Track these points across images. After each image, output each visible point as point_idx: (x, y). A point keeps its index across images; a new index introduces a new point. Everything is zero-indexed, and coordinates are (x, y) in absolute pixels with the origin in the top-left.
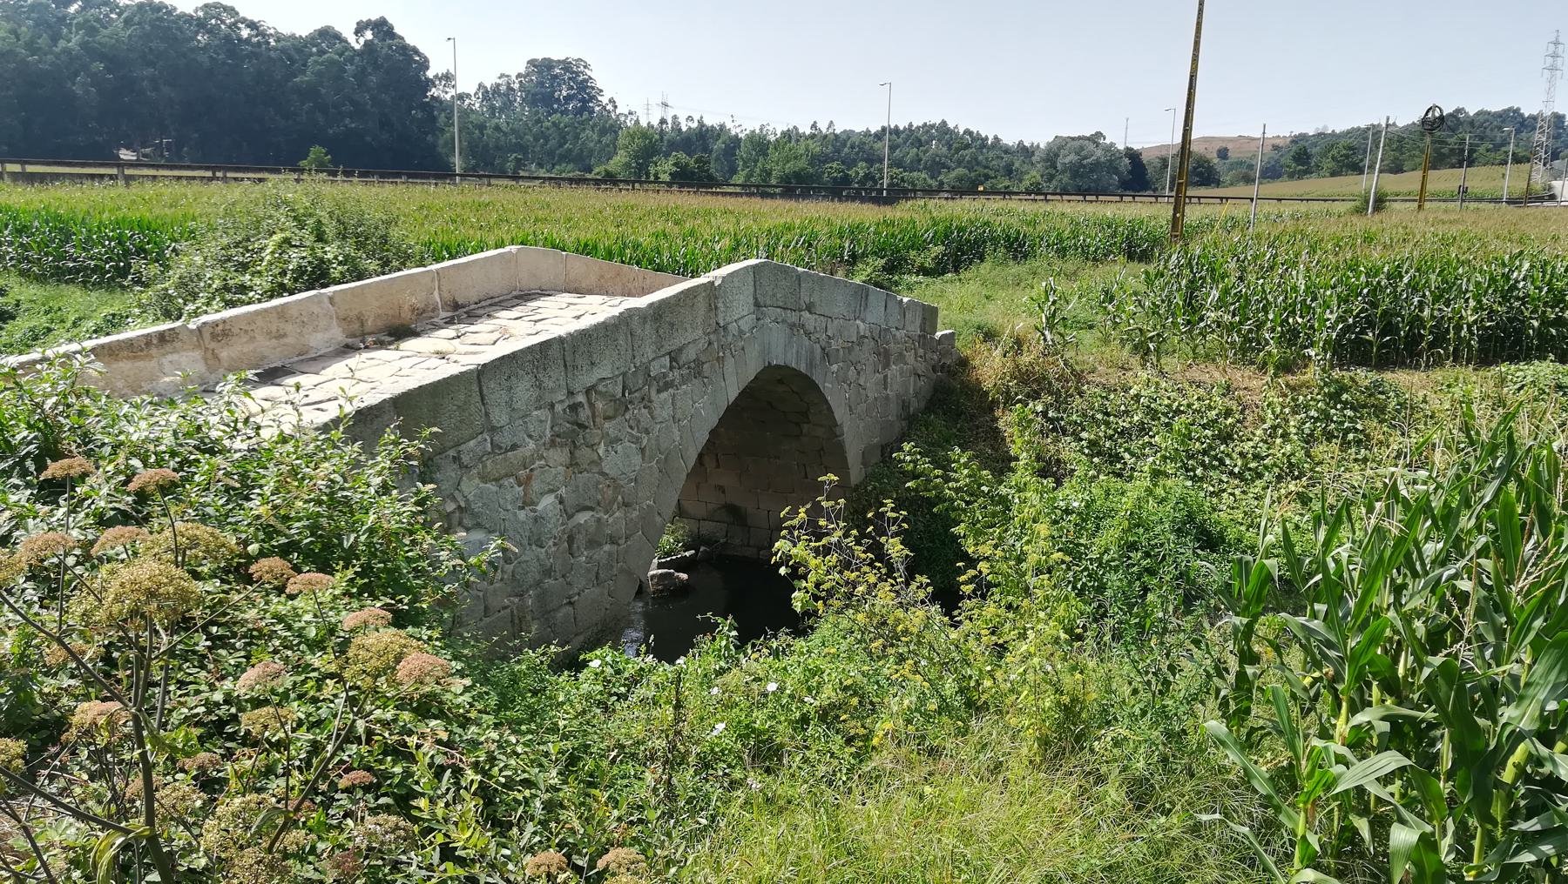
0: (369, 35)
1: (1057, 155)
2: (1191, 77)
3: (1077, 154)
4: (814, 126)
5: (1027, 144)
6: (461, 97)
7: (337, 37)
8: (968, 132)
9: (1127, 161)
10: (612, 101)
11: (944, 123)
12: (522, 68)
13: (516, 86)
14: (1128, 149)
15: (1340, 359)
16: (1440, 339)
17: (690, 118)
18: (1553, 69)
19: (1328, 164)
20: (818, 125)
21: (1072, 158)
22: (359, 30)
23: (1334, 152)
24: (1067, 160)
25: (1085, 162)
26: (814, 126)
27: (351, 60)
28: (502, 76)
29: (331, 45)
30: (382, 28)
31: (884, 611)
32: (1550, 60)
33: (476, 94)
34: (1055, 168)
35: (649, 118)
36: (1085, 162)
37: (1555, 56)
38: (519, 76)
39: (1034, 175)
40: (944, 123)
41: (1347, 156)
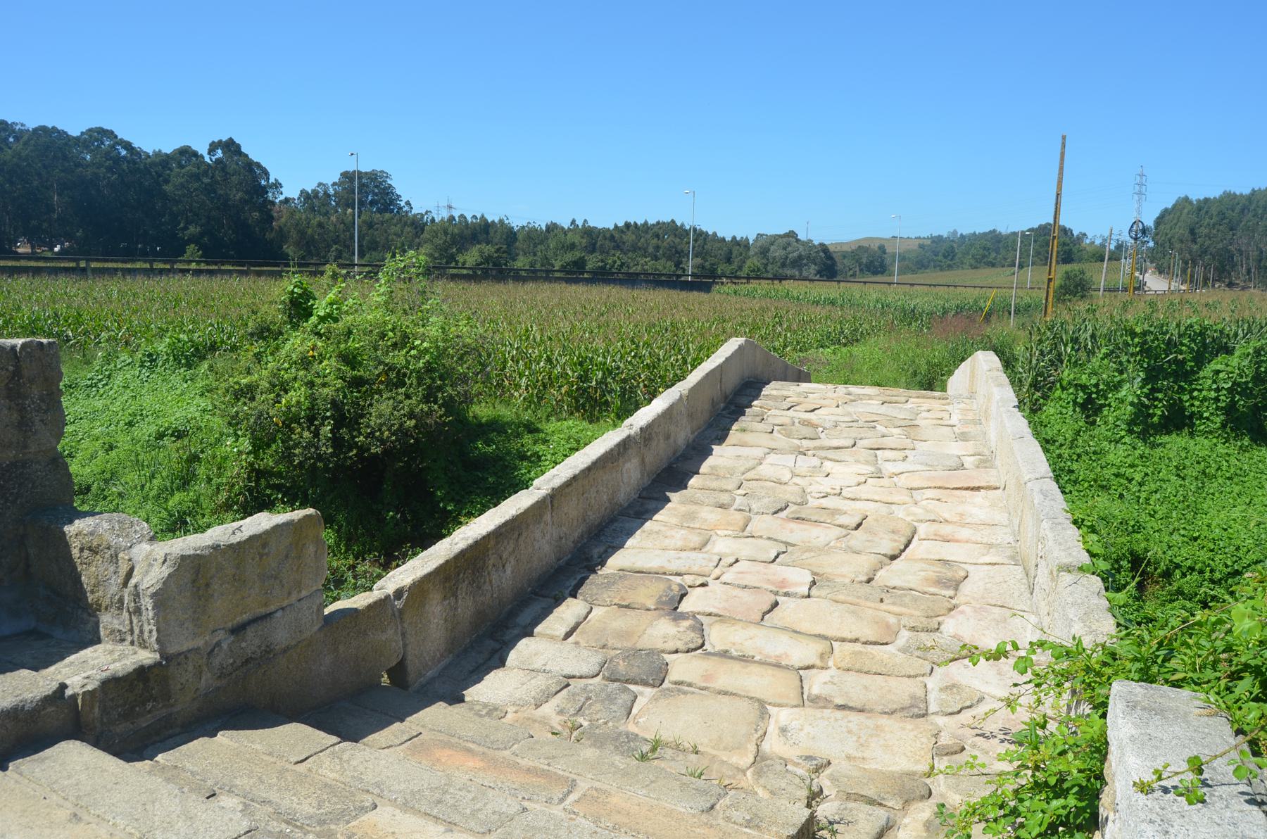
0: (219, 154)
2: (1057, 204)
4: (573, 222)
6: (287, 200)
7: (195, 154)
10: (408, 203)
12: (336, 178)
13: (331, 191)
14: (822, 245)
16: (399, 673)
17: (474, 217)
18: (1140, 193)
19: (969, 260)
20: (577, 223)
22: (212, 150)
26: (573, 222)
27: (205, 173)
28: (320, 184)
29: (189, 160)
30: (231, 147)
31: (1235, 535)
32: (1137, 187)
33: (299, 198)
35: (441, 215)
37: (1141, 185)
38: (334, 184)
39: (754, 262)
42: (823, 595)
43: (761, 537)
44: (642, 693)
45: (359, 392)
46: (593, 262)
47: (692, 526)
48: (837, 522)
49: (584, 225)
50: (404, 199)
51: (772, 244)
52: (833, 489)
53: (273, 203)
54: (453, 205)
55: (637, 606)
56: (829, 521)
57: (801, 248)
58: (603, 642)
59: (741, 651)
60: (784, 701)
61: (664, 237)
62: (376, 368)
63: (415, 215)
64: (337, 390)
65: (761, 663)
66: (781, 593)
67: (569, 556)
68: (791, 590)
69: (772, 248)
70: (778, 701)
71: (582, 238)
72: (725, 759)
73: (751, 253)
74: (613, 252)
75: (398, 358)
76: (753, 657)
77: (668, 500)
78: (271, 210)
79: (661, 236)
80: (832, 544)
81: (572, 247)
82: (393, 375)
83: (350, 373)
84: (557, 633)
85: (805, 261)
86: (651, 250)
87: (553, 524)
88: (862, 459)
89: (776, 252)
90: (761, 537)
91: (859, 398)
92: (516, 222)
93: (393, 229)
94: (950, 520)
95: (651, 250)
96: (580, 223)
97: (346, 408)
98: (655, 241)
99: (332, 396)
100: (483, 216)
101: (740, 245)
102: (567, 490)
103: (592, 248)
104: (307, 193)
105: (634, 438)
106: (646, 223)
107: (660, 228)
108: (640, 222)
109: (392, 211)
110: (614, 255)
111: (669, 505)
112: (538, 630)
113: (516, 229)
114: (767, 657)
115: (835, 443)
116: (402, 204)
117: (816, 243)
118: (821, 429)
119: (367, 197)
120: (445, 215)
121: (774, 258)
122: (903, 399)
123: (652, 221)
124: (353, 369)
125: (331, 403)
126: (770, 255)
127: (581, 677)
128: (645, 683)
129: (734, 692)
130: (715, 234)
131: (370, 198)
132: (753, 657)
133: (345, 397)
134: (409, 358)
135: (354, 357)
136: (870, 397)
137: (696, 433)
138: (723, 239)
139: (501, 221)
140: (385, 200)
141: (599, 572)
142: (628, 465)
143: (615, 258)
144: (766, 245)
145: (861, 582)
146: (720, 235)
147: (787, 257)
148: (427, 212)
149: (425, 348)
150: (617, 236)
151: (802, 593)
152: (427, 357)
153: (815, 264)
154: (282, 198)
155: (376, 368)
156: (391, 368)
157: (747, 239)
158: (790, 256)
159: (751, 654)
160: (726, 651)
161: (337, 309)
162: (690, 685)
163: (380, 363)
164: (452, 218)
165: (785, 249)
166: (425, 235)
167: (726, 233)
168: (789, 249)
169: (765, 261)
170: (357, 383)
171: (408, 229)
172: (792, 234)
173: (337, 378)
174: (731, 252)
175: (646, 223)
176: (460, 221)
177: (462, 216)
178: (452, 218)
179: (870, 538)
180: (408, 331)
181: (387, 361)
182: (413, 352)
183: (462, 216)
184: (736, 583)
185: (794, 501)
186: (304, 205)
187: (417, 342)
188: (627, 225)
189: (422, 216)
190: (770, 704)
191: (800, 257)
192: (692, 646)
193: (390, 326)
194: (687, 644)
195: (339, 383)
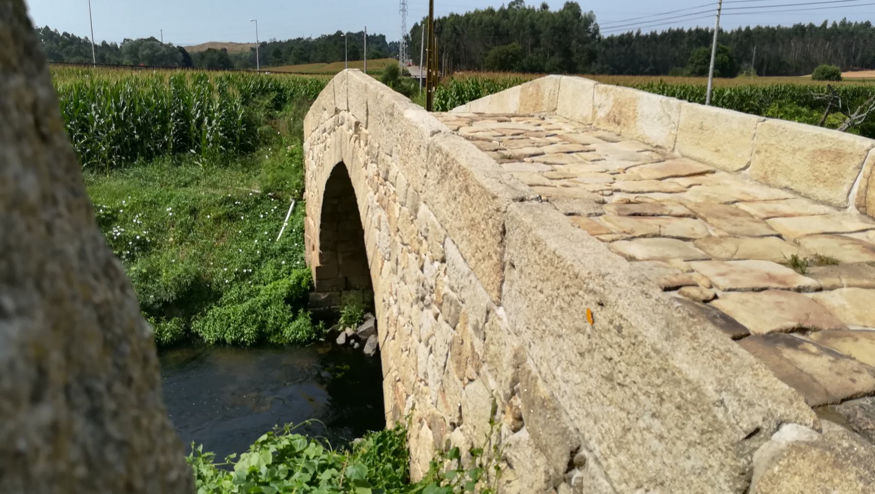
1: (137, 50)
3: (150, 49)
5: (109, 43)
8: (65, 34)
9: (181, 54)
11: (47, 28)
15: (125, 239)
19: (292, 57)
21: (147, 52)
23: (294, 51)
24: (145, 53)
25: (156, 54)
34: (137, 57)
36: (156, 54)
40: (47, 28)
41: (301, 54)
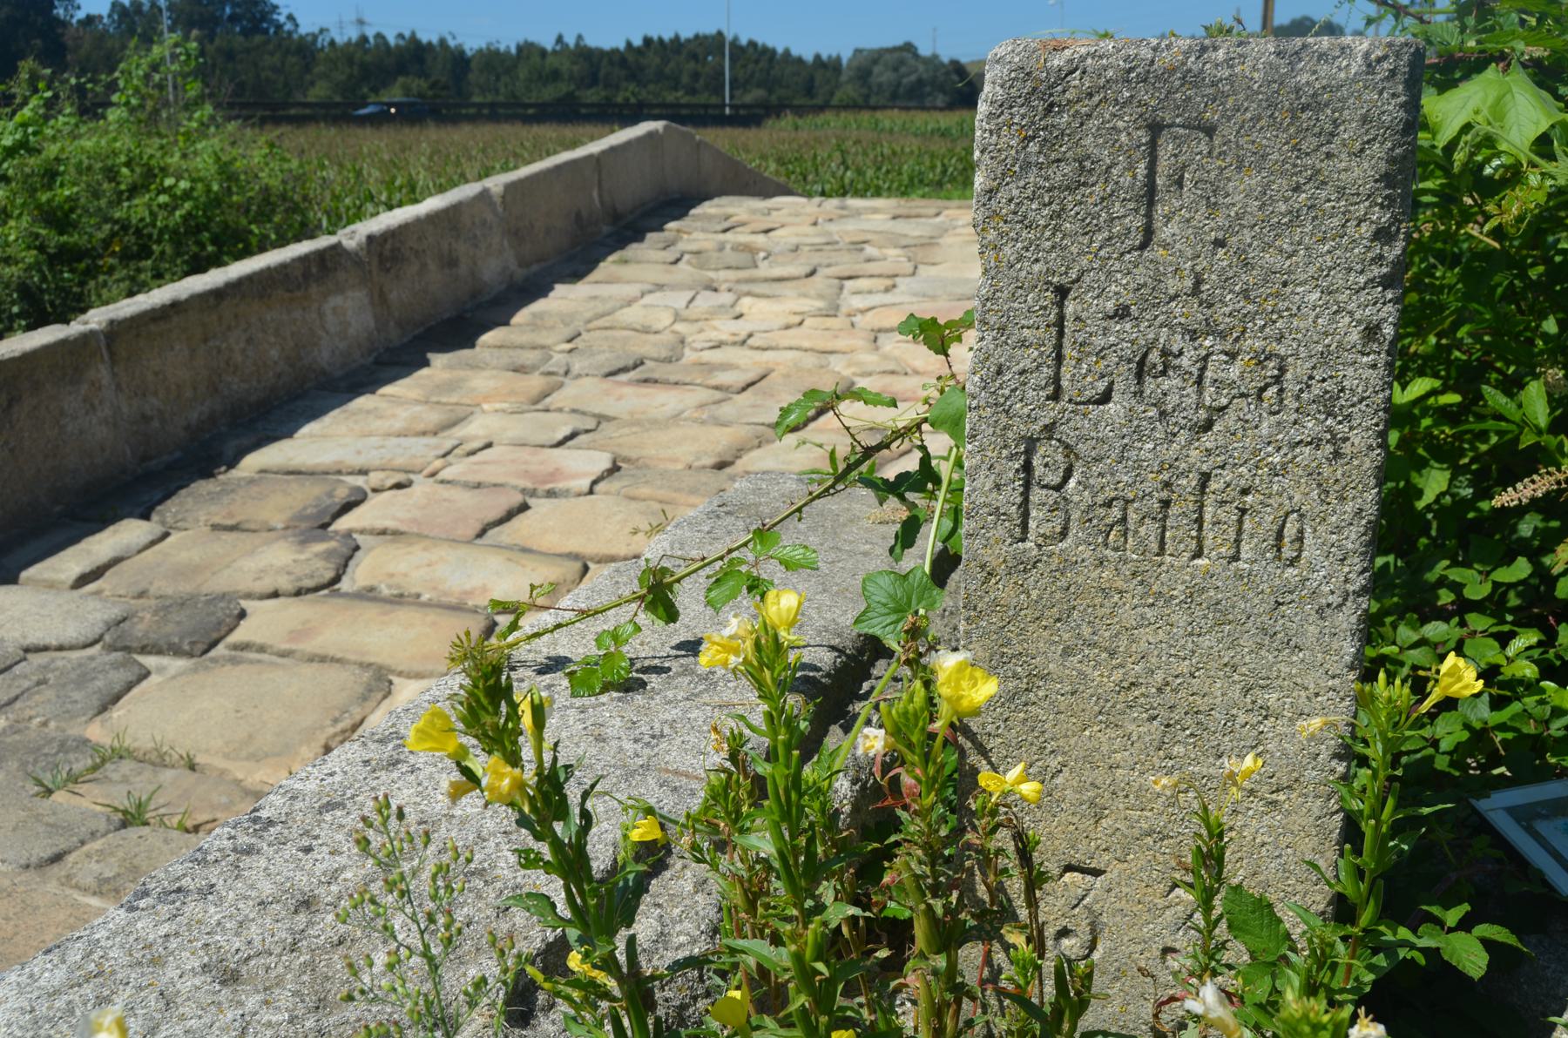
4: (560, 39)
6: (90, 20)
10: (290, 18)
17: (401, 36)
26: (560, 39)
33: (110, 16)
35: (345, 34)
39: (849, 91)
42: (613, 490)
43: (560, 410)
44: (161, 670)
45: (72, 271)
46: (592, 96)
47: (444, 400)
48: (713, 382)
49: (577, 45)
50: (284, 12)
51: (875, 62)
52: (734, 335)
53: (64, 24)
54: (367, 19)
55: (253, 526)
56: (698, 381)
57: (921, 68)
58: (139, 588)
59: (398, 587)
60: (429, 667)
61: (705, 58)
62: (100, 228)
63: (302, 38)
64: (29, 269)
65: (429, 605)
66: (540, 492)
67: (178, 454)
68: (560, 485)
69: (876, 70)
70: (417, 667)
71: (574, 63)
72: (240, 776)
73: (844, 78)
74: (624, 84)
75: (138, 209)
76: (418, 596)
77: (426, 363)
78: (63, 35)
79: (701, 57)
80: (686, 414)
81: (555, 75)
82: (130, 239)
83: (54, 239)
84: (62, 577)
85: (928, 89)
86: (685, 79)
87: (119, 387)
88: (812, 292)
89: (882, 76)
90: (560, 410)
91: (858, 213)
92: (472, 41)
93: (268, 61)
94: (921, 370)
95: (685, 79)
96: (570, 40)
97: (47, 297)
98: (692, 65)
99: (19, 277)
100: (413, 34)
101: (827, 67)
102: (153, 327)
103: (592, 79)
104: (123, 6)
105: (357, 254)
106: (677, 38)
107: (700, 44)
108: (667, 36)
109: (266, 31)
110: (626, 90)
111: (424, 372)
112: (24, 575)
113: (469, 53)
114: (445, 594)
115: (778, 272)
116: (282, 19)
117: (945, 58)
118: (762, 255)
119: (224, 9)
120: (353, 34)
121: (880, 85)
122: (932, 211)
123: (686, 34)
124: (61, 234)
125: (17, 290)
126: (874, 80)
127: (60, 648)
128: (177, 651)
129: (339, 655)
130: (787, 53)
131: (228, 10)
132: (418, 596)
133: (44, 279)
134: (155, 208)
135: (67, 215)
136: (875, 211)
137: (535, 268)
138: (800, 61)
139: (443, 42)
140: (254, 15)
141: (221, 477)
142: (336, 301)
143: (628, 94)
144: (867, 64)
145: (704, 467)
146: (795, 52)
147: (899, 84)
148: (322, 31)
149: (185, 190)
150: (631, 58)
151: (577, 490)
152: (188, 205)
153: (945, 93)
154: (81, 15)
155: (100, 228)
156: (125, 226)
157: (839, 59)
158: (905, 81)
159: (414, 590)
160: (372, 589)
161: (35, 134)
162: (262, 649)
163: (107, 220)
164: (364, 39)
165: (896, 69)
166: (319, 69)
167: (805, 49)
168: (903, 70)
169: (865, 91)
170: (67, 256)
171: (292, 59)
172: (909, 48)
173: (29, 248)
174: (812, 79)
175: (677, 38)
176: (377, 45)
177: (379, 36)
178: (364, 39)
179: (759, 402)
180: (153, 162)
181: (117, 215)
182: (163, 199)
183: (379, 36)
184: (463, 479)
185: (655, 355)
186: (119, 26)
187: (169, 182)
188: (648, 41)
189: (315, 37)
190: (400, 674)
191: (920, 82)
192: (309, 583)
193: (123, 159)
194: (300, 579)
195: (30, 256)
